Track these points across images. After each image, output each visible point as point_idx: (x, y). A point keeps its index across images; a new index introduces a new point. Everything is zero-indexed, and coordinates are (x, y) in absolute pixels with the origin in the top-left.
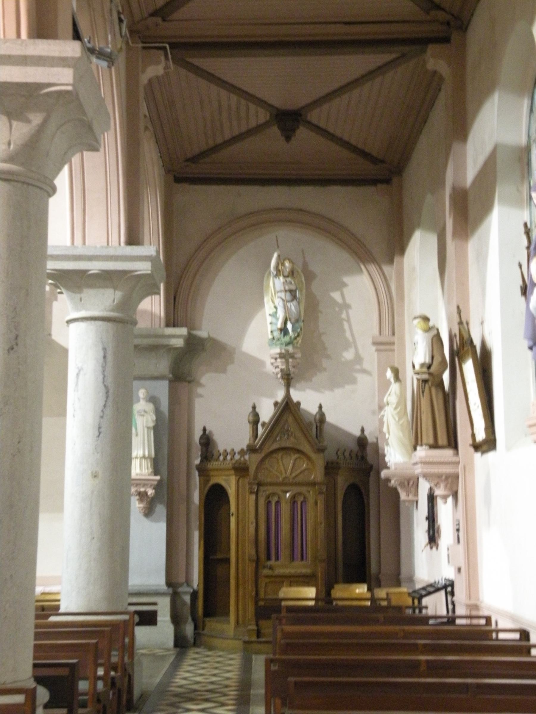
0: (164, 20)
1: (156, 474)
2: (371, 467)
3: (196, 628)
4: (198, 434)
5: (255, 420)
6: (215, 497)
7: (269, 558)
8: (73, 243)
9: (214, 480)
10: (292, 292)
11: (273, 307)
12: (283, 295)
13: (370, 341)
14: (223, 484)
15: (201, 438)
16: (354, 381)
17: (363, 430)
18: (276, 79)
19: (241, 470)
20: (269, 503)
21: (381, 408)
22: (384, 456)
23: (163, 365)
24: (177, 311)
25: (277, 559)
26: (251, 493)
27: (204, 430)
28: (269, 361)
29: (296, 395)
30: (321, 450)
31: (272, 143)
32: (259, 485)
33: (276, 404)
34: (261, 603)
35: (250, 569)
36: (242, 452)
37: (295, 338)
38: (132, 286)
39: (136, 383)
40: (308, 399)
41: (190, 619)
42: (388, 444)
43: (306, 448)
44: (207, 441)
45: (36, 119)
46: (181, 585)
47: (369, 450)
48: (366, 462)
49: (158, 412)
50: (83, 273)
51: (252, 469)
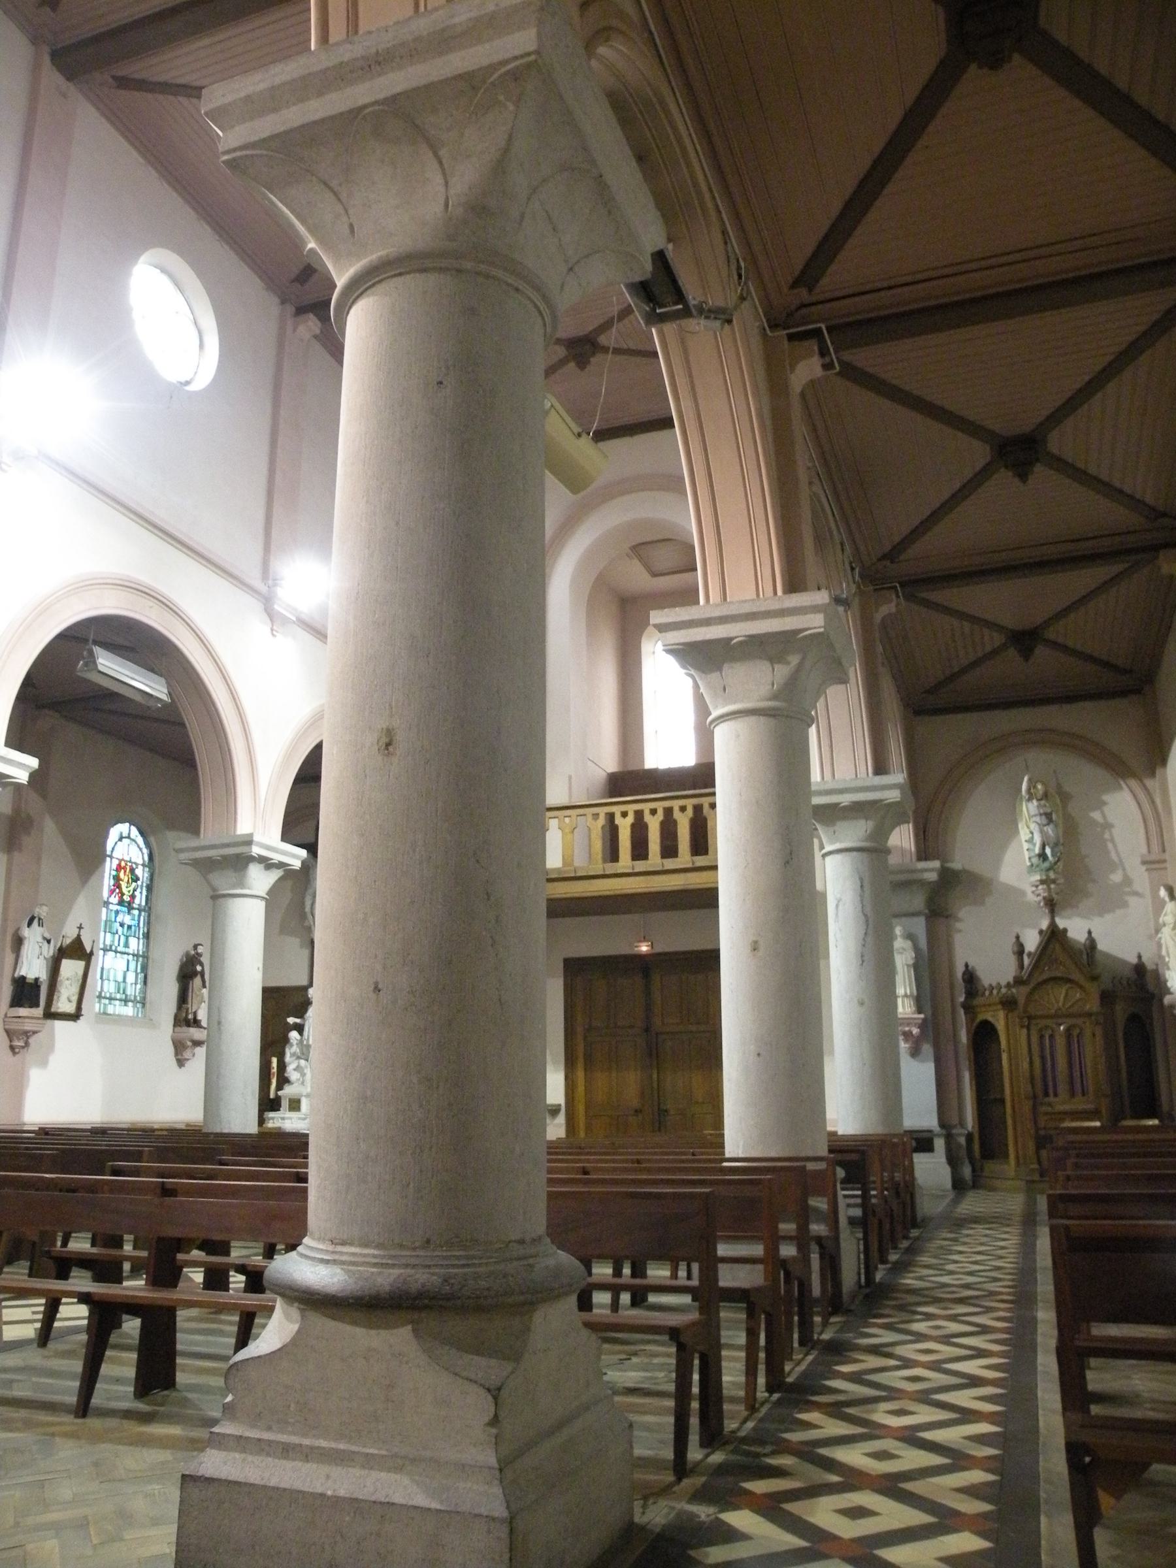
0: (892, 562)
1: (920, 1012)
2: (1153, 996)
3: (974, 1171)
4: (960, 970)
5: (1020, 951)
6: (984, 1035)
7: (1046, 1094)
8: (823, 778)
9: (981, 1017)
10: (1048, 816)
11: (1029, 834)
12: (1038, 819)
13: (1139, 860)
14: (990, 1019)
15: (964, 974)
16: (1125, 905)
17: (1140, 957)
18: (1004, 602)
19: (1009, 1004)
20: (1042, 1037)
21: (1157, 931)
22: (1166, 981)
23: (918, 901)
24: (927, 847)
25: (1056, 1095)
26: (1022, 1027)
27: (967, 965)
28: (1029, 890)
29: (1061, 923)
30: (1095, 978)
31: (1011, 663)
32: (1030, 1018)
33: (1041, 932)
34: (1042, 1133)
35: (1027, 1106)
36: (1008, 985)
37: (1056, 863)
38: (881, 816)
39: (895, 921)
40: (1076, 928)
41: (967, 1161)
42: (1168, 969)
43: (1076, 976)
44: (970, 977)
45: (794, 660)
46: (955, 1126)
47: (1149, 978)
48: (1147, 992)
49: (916, 948)
50: (834, 807)
51: (1021, 1001)
